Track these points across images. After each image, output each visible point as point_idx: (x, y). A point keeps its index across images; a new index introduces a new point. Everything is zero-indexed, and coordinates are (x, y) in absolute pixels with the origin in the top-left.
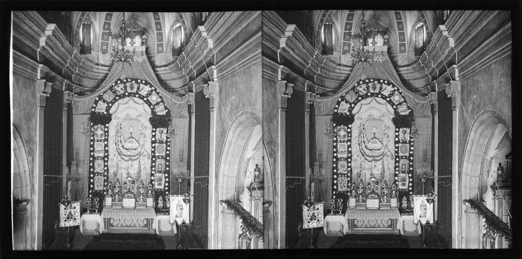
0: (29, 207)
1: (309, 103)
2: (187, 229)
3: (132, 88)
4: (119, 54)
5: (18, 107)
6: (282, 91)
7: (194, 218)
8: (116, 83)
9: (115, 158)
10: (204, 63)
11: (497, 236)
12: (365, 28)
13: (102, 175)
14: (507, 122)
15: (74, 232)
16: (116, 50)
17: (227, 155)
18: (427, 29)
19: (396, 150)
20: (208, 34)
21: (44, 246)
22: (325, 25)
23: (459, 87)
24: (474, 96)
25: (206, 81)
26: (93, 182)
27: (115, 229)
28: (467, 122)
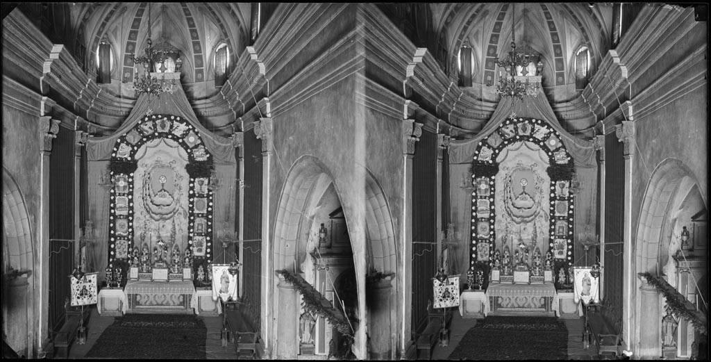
0: (394, 282)
1: (442, 148)
2: (235, 308)
3: (524, 130)
4: (509, 86)
5: (379, 155)
6: (409, 131)
7: (605, 296)
8: (504, 123)
9: (503, 220)
10: (617, 97)
11: (317, 317)
12: (151, 50)
13: (126, 238)
14: (697, 175)
15: (90, 313)
16: (504, 81)
17: (647, 216)
18: (231, 51)
19: (191, 206)
20: (258, 57)
21: (414, 333)
22: (101, 45)
23: (271, 126)
24: (654, 141)
25: (620, 120)
26: (476, 250)
27: (504, 311)
28: (281, 171)
